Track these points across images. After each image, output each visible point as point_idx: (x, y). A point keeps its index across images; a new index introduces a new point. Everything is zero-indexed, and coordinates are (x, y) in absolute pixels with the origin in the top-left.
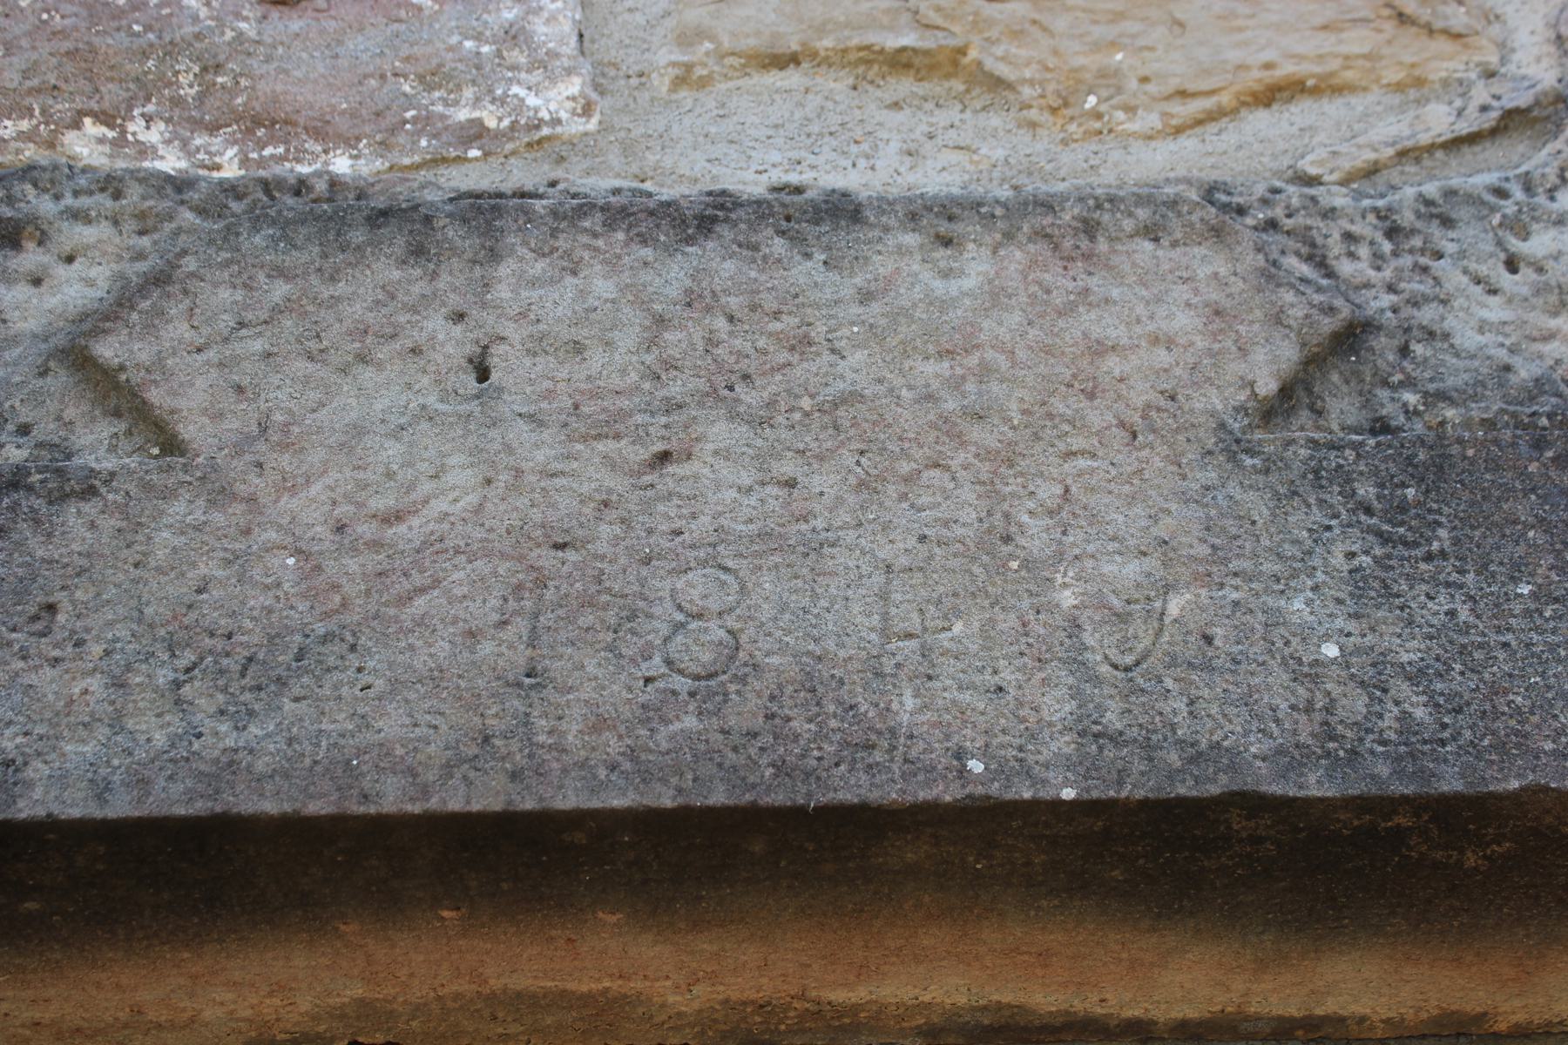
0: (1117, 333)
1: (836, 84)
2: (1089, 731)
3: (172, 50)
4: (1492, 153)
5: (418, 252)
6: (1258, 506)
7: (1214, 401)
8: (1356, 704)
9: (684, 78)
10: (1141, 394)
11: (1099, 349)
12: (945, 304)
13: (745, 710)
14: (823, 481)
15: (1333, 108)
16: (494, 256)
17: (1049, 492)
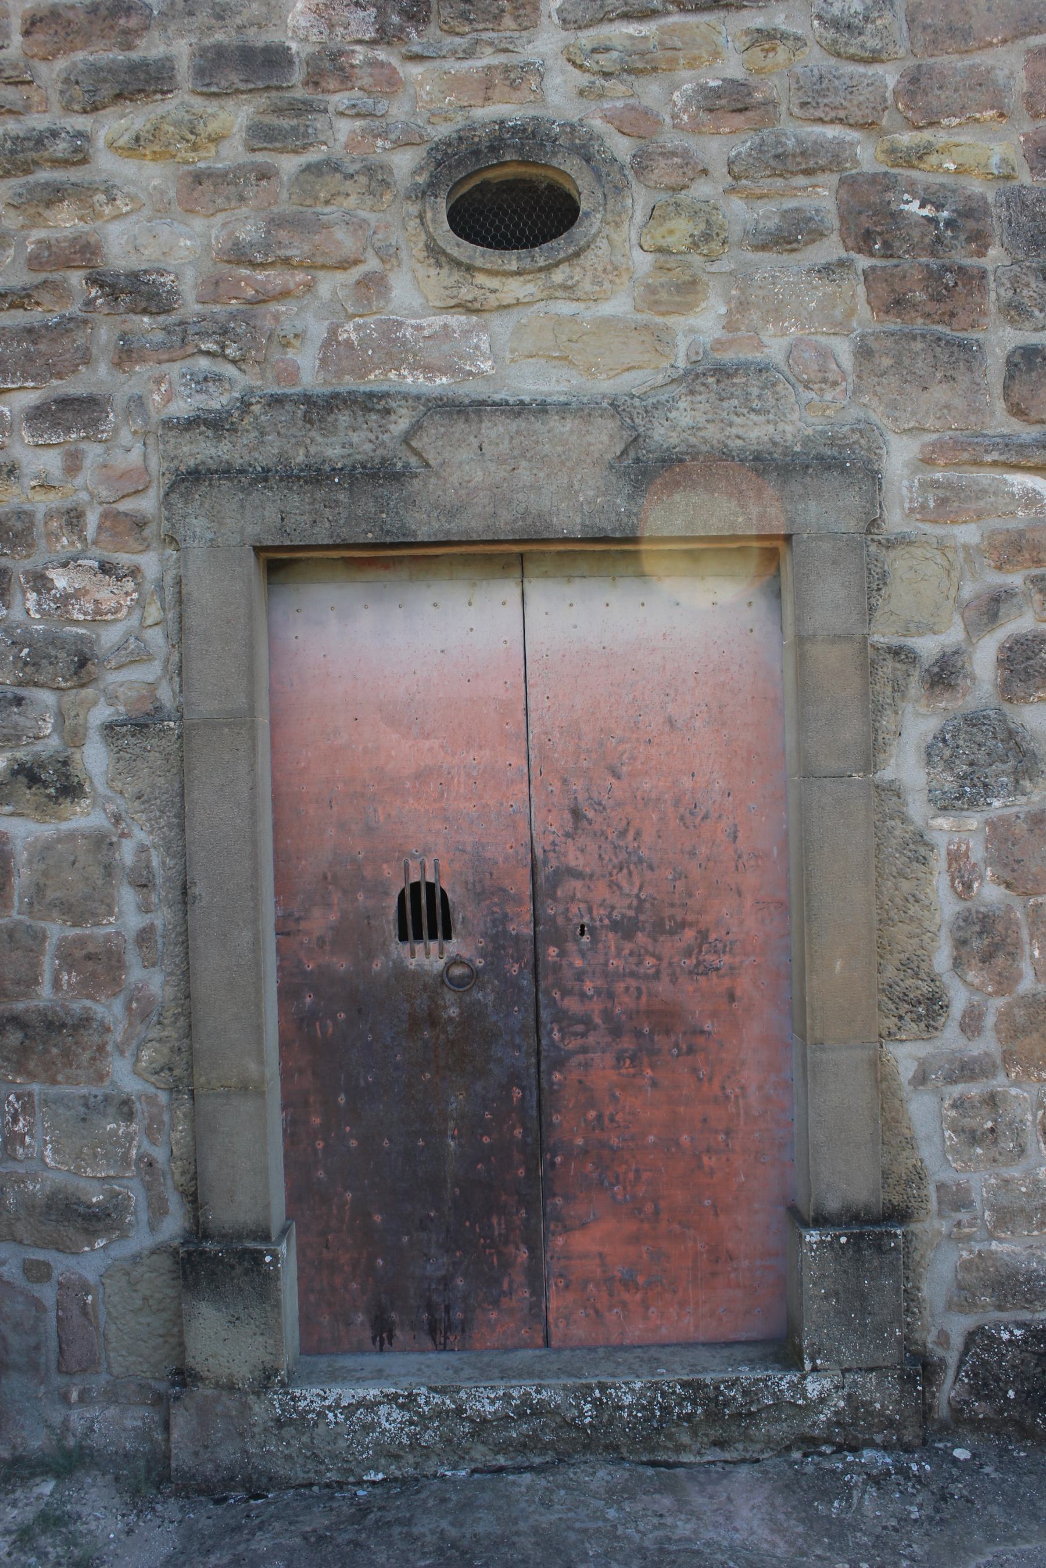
0: (593, 441)
1: (543, 361)
2: (583, 525)
3: (407, 352)
4: (669, 388)
5: (467, 421)
6: (614, 479)
7: (609, 457)
8: (625, 520)
9: (512, 360)
10: (596, 455)
11: (590, 444)
12: (563, 434)
13: (529, 521)
14: (541, 475)
15: (640, 372)
16: (481, 422)
17: (579, 477)
